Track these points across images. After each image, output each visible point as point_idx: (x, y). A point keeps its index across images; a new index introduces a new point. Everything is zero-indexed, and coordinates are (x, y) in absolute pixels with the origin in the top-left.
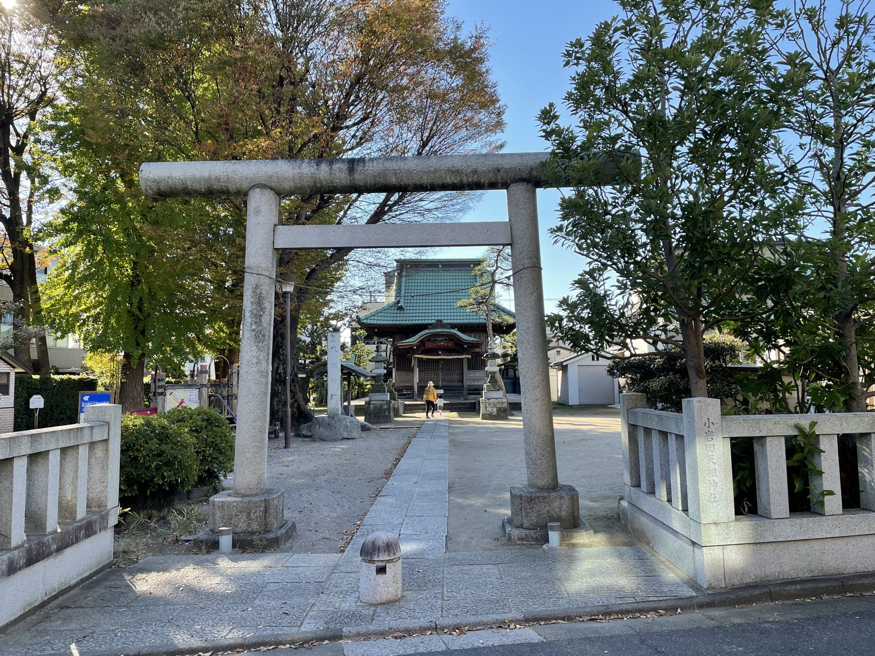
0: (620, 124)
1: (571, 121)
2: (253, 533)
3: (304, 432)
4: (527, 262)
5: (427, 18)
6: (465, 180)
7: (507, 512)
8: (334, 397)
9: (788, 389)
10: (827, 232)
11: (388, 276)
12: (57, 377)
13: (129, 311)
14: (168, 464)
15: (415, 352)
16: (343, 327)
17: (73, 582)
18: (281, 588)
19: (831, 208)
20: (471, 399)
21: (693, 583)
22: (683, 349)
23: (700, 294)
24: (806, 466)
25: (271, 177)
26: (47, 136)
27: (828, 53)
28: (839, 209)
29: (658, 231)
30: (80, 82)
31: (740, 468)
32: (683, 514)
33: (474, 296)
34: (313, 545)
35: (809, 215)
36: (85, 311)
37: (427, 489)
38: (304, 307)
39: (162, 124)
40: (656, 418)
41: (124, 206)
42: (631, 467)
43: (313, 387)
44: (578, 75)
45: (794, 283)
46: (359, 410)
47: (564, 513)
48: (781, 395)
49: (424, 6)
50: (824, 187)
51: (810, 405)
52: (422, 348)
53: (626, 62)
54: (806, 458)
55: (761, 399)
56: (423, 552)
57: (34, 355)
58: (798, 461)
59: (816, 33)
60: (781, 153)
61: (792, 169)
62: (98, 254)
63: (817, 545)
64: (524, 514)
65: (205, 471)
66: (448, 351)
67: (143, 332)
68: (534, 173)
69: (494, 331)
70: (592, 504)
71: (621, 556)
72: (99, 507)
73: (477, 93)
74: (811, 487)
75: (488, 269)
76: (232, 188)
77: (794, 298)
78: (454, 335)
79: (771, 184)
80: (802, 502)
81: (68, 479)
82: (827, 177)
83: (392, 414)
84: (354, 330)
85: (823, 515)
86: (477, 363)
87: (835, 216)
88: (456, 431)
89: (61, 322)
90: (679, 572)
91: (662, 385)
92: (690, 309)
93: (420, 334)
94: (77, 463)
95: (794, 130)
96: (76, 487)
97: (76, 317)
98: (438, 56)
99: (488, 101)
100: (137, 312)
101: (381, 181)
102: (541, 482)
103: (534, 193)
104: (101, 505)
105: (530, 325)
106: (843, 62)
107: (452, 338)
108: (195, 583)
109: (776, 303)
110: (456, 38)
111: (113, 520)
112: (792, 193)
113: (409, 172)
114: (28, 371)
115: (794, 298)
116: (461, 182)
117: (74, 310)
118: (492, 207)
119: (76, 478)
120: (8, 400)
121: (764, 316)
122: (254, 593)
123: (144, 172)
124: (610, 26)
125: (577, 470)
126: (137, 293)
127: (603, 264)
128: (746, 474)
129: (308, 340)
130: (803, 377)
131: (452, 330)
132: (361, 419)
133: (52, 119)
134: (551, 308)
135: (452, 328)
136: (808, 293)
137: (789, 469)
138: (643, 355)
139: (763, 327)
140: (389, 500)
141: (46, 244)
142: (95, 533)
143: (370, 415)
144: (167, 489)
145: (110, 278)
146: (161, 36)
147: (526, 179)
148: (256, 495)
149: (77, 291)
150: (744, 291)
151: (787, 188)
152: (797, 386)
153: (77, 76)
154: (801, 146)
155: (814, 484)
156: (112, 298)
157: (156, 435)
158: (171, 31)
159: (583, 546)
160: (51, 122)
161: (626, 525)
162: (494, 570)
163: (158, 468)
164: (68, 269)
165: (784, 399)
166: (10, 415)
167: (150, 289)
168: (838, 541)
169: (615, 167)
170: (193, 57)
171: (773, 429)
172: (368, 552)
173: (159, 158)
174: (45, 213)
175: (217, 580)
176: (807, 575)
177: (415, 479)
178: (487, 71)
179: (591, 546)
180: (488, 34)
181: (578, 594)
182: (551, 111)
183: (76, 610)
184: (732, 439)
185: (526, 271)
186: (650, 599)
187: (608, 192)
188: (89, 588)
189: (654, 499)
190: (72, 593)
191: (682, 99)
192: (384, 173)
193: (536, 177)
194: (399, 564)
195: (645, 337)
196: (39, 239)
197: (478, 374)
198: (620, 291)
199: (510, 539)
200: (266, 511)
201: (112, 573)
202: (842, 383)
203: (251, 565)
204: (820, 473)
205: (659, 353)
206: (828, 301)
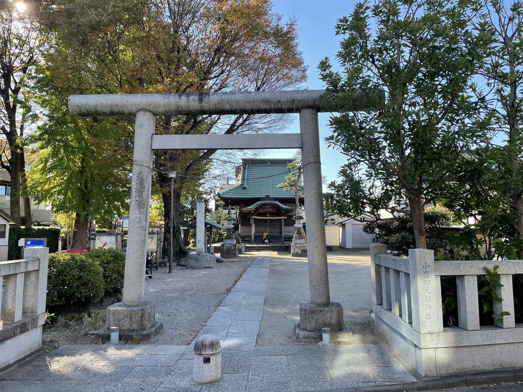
0: (369, 69)
1: (340, 69)
2: (133, 330)
3: (182, 263)
4: (311, 159)
5: (259, 12)
6: (273, 107)
7: (297, 318)
9: (480, 242)
10: (505, 141)
11: (238, 169)
12: (36, 228)
13: (79, 188)
14: (85, 284)
17: (11, 362)
18: (143, 370)
19: (508, 126)
20: (286, 244)
21: (415, 373)
22: (411, 217)
23: (421, 181)
24: (491, 295)
25: (150, 104)
26: (32, 83)
27: (506, 27)
28: (513, 126)
29: (396, 140)
30: (52, 51)
31: (448, 296)
32: (409, 325)
33: (288, 181)
34: (172, 339)
35: (494, 129)
36: (53, 188)
37: (251, 302)
38: (184, 187)
39: (101, 76)
40: (392, 262)
41: (77, 125)
42: (377, 292)
43: (192, 235)
44: (345, 40)
45: (483, 173)
46: (217, 250)
47: (333, 322)
48: (475, 247)
49: (258, 5)
50: (504, 113)
51: (494, 253)
52: (257, 212)
53: (373, 27)
54: (491, 290)
55: (462, 249)
56: (240, 345)
57: (22, 214)
58: (486, 292)
59: (499, 14)
60: (476, 91)
61: (482, 100)
62: (60, 154)
63: (497, 348)
64: (307, 321)
65: (112, 288)
66: (273, 214)
67: (87, 201)
68: (317, 103)
69: (300, 202)
70: (354, 313)
71: (368, 351)
72: (32, 313)
73: (289, 57)
74: (495, 309)
75: (296, 164)
76: (126, 111)
77: (484, 183)
78: (276, 205)
79: (470, 109)
80: (488, 319)
81: (10, 295)
82: (505, 105)
83: (237, 252)
84: (217, 201)
85: (502, 328)
86: (290, 222)
87: (511, 130)
88: (275, 263)
89: (38, 195)
90: (406, 364)
91: (397, 238)
92: (415, 190)
94: (16, 285)
95: (484, 75)
96: (15, 301)
97: (48, 191)
98: (266, 35)
99: (297, 64)
100: (84, 189)
101: (220, 107)
102: (319, 301)
103: (317, 115)
104: (33, 312)
105: (313, 199)
106: (516, 32)
107: (275, 206)
108: (89, 365)
109: (472, 187)
110: (278, 25)
111: (41, 322)
112: (483, 116)
113: (237, 101)
114: (17, 224)
115: (484, 183)
116: (270, 108)
117: (47, 187)
118: (293, 124)
119: (15, 295)
120: (5, 241)
121: (464, 195)
122: (125, 373)
123: (71, 101)
124: (363, 6)
125: (347, 290)
126: (83, 177)
127: (358, 160)
128: (452, 299)
129: (190, 207)
130: (490, 235)
131: (275, 202)
132: (218, 255)
133: (35, 73)
134: (325, 190)
135: (275, 200)
136: (492, 180)
137: (480, 297)
138: (386, 220)
139: (464, 203)
140: (226, 309)
141: (30, 147)
142: (28, 330)
143: (224, 253)
144: (84, 300)
145: (68, 168)
146: (99, 23)
147: (312, 106)
148: (137, 306)
149: (48, 176)
150: (450, 179)
151: (479, 112)
152: (485, 241)
153: (51, 47)
154: (488, 84)
155: (496, 306)
156: (69, 181)
157: (77, 266)
158: (105, 19)
159: (345, 343)
160: (34, 75)
161: (374, 330)
162: (284, 359)
163: (78, 287)
164: (42, 163)
165: (477, 249)
166: (6, 250)
167: (92, 175)
168: (512, 346)
169: (368, 99)
170: (119, 36)
171: (469, 271)
172: (199, 348)
173: (82, 92)
174: (31, 129)
175: (103, 363)
176: (491, 368)
177: (244, 295)
178: (296, 46)
179: (350, 343)
180: (297, 23)
181: (338, 379)
182: (326, 62)
183: (9, 382)
184: (441, 276)
185: (311, 165)
186: (386, 384)
187: (361, 115)
188: (21, 366)
189: (391, 314)
190: (11, 369)
191: (411, 55)
192: (221, 102)
193: (318, 105)
194: (219, 357)
195: (386, 208)
196: (25, 145)
197: (290, 228)
198: (367, 178)
199: (298, 338)
200: (142, 317)
201: (39, 356)
202: (515, 240)
203: (128, 353)
204: (501, 300)
205: (395, 218)
206: (506, 186)
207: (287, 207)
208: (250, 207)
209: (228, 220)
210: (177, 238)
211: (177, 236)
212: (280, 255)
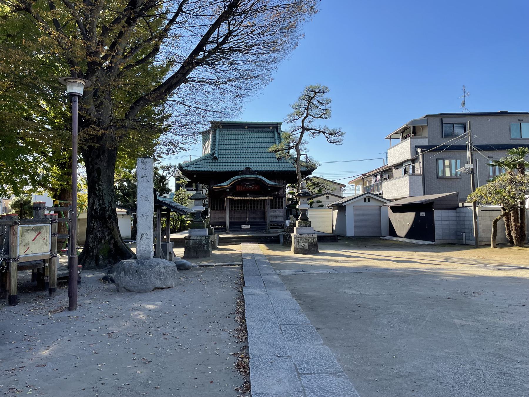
8: (145, 237)
15: (228, 194)
16: (169, 176)
52: (234, 190)
66: (254, 193)
131: (258, 176)
208: (224, 184)
209: (196, 199)
210: (109, 229)
211: (109, 225)
212: (274, 250)
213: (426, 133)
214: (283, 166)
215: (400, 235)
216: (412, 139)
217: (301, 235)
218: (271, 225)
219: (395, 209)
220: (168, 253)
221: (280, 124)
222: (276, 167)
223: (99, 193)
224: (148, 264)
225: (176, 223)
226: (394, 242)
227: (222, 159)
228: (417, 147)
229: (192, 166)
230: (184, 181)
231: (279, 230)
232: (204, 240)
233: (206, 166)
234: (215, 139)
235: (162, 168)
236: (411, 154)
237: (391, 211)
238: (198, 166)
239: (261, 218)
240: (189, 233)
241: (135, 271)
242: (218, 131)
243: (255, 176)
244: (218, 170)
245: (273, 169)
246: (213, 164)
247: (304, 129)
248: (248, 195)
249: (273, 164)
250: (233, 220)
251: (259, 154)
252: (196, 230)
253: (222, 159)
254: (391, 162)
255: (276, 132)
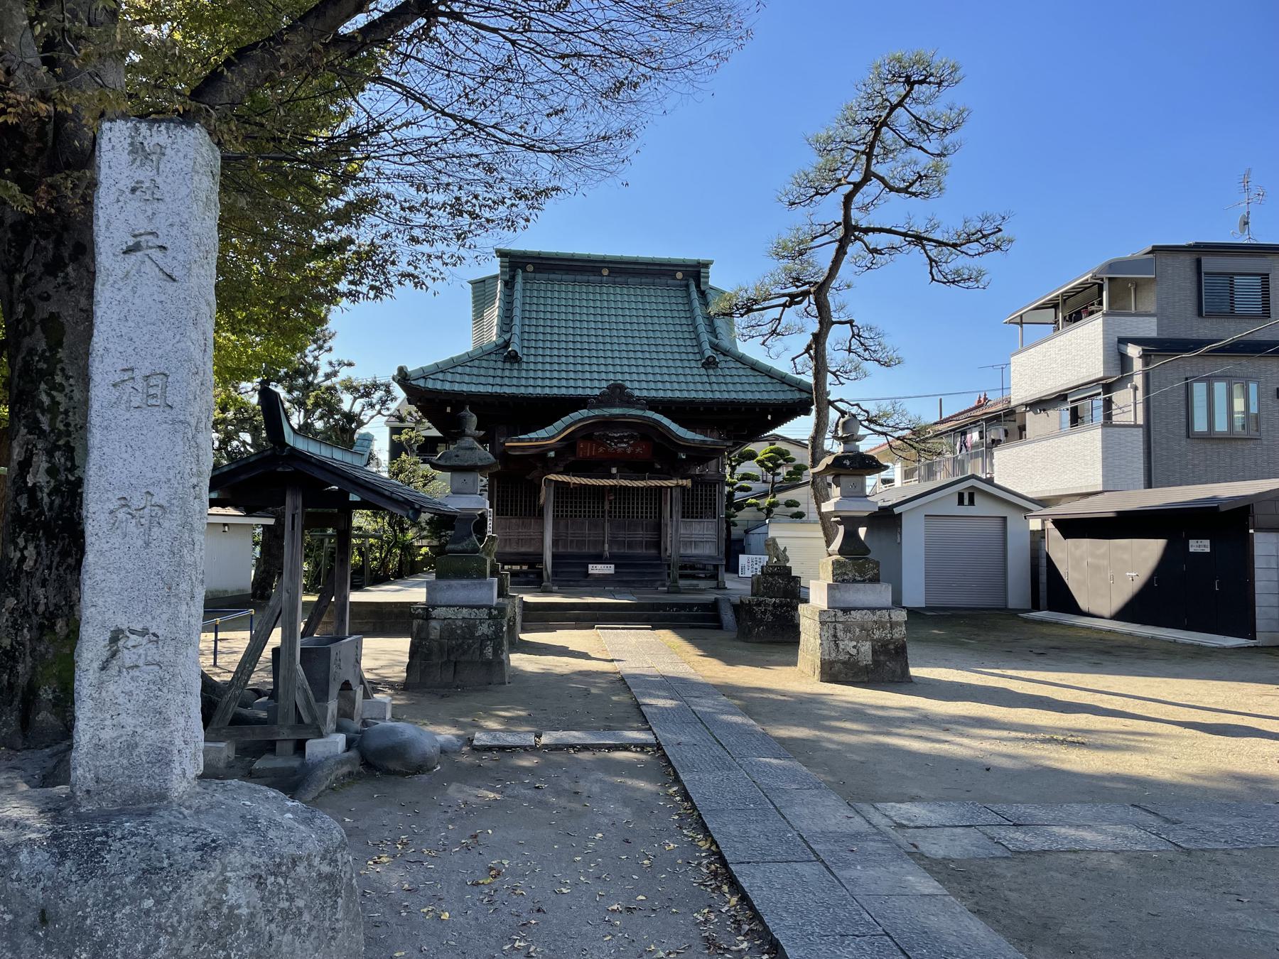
11: (481, 289)
15: (550, 466)
16: (370, 412)
52: (570, 454)
66: (633, 467)
93: (567, 419)
131: (650, 414)
207: (699, 437)
208: (542, 433)
212: (730, 661)
213: (1149, 302)
214: (724, 387)
215: (1093, 610)
216: (1111, 319)
217: (846, 610)
218: (683, 567)
219: (1072, 528)
220: (334, 690)
221: (706, 265)
222: (700, 387)
223: (53, 420)
224: (135, 858)
225: (389, 551)
226: (1083, 633)
227: (532, 359)
228: (1123, 341)
229: (440, 376)
230: (413, 434)
231: (702, 584)
232: (482, 621)
233: (483, 380)
234: (511, 303)
235: (350, 388)
236: (1105, 362)
237: (1057, 533)
238: (458, 378)
239: (648, 545)
240: (431, 589)
241: (31, 916)
242: (519, 279)
243: (639, 413)
244: (522, 390)
245: (693, 395)
246: (507, 373)
247: (850, 231)
248: (614, 470)
249: (690, 379)
250: (561, 550)
251: (626, 369)
252: (454, 582)
253: (532, 359)
254: (1021, 392)
255: (693, 288)
